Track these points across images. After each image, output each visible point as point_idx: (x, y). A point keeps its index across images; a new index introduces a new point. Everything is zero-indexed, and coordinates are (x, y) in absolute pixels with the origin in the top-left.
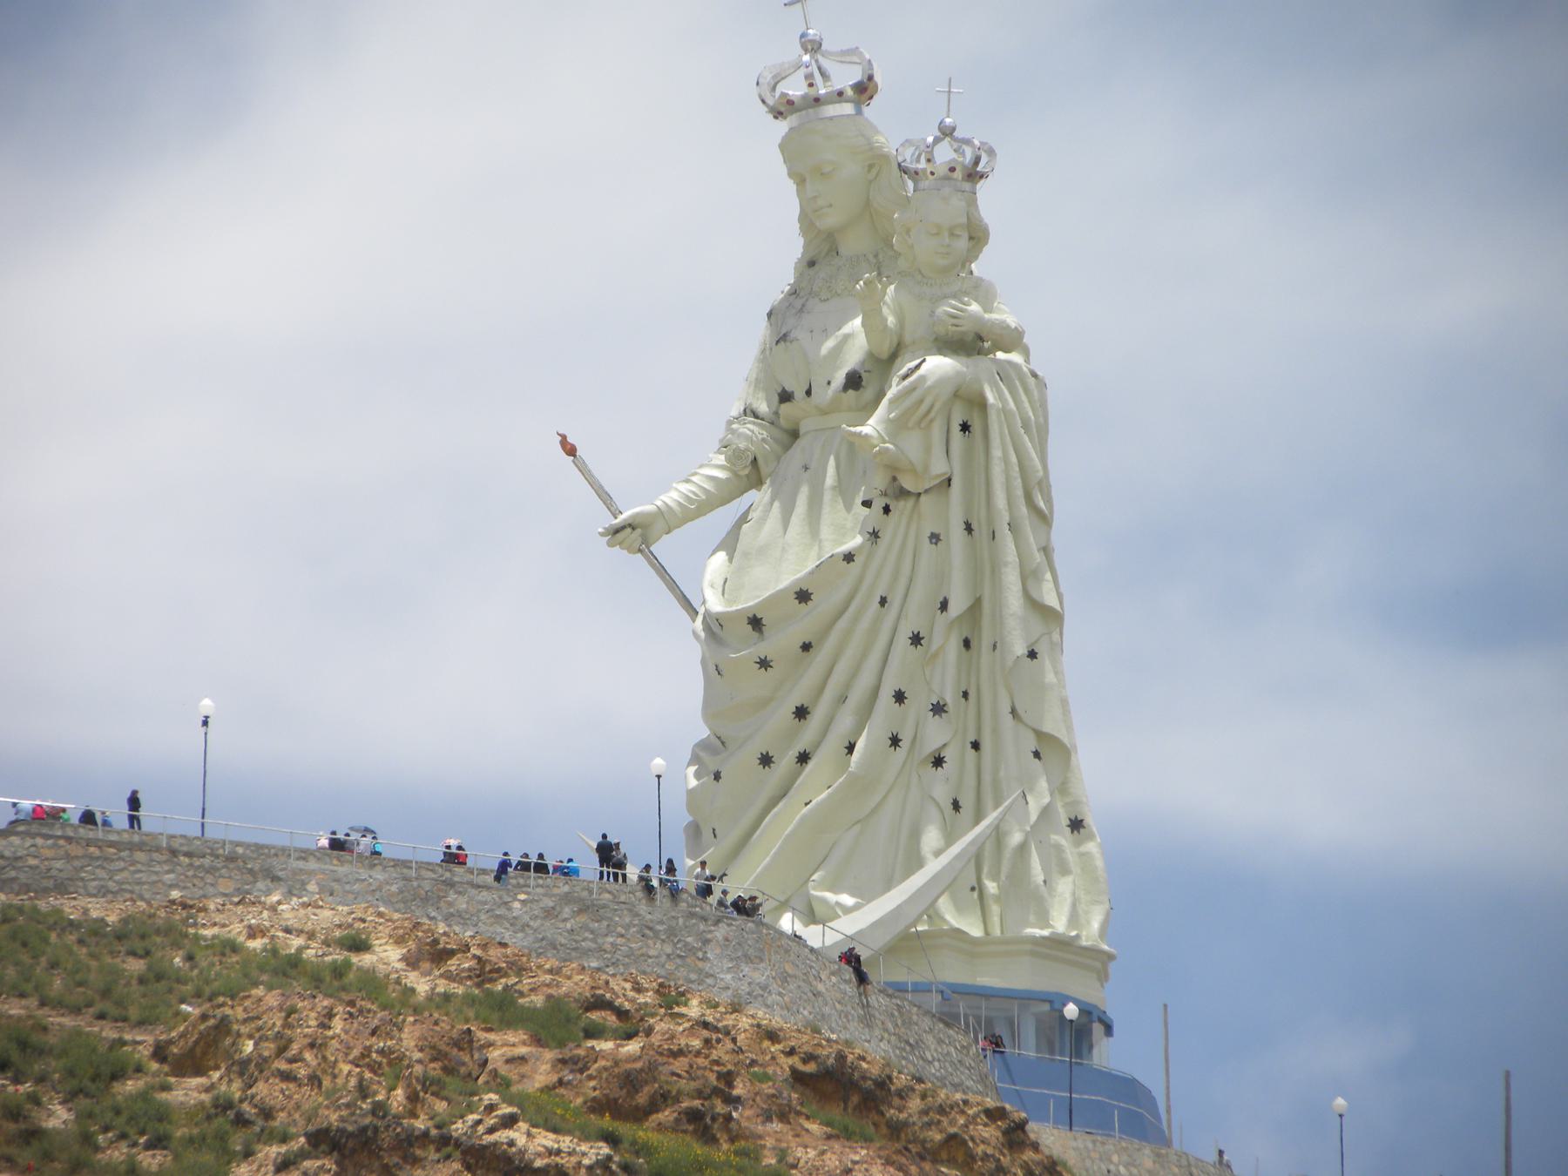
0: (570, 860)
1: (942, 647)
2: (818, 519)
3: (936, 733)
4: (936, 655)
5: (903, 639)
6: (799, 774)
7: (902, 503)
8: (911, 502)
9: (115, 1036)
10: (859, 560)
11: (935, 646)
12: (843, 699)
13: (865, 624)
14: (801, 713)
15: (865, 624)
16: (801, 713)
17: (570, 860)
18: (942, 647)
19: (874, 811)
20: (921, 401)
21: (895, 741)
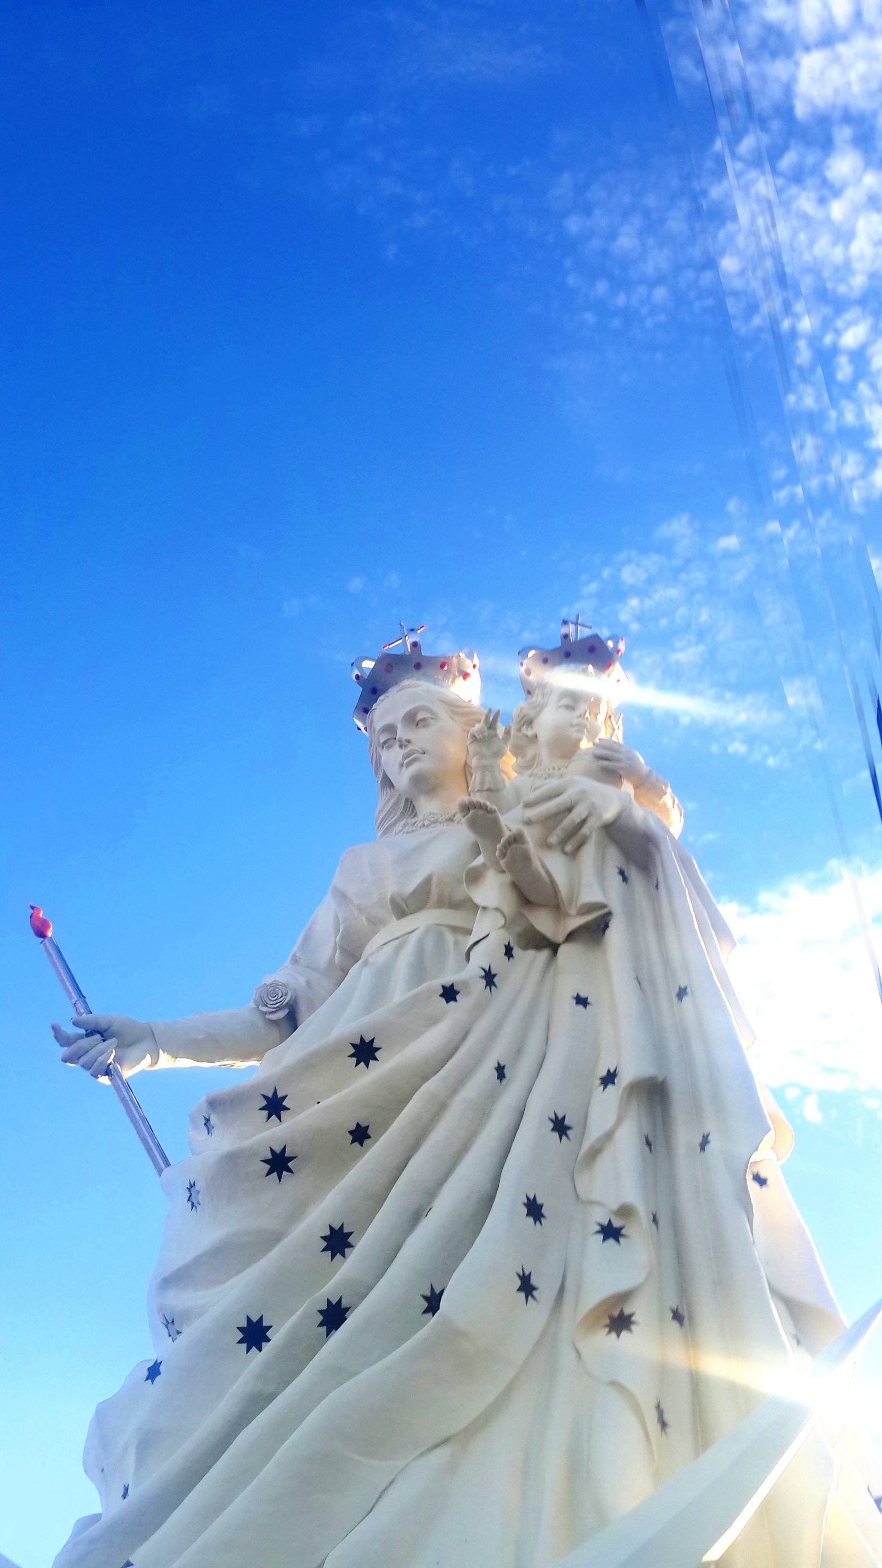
0: (761, 1181)
1: (609, 1136)
2: (868, 759)
3: (606, 1272)
4: (595, 1153)
5: (534, 1127)
6: (313, 1350)
7: (531, 953)
8: (545, 954)
9: (803, 289)
10: (463, 1002)
11: (595, 1132)
12: (416, 1217)
13: (471, 1090)
14: (337, 1242)
15: (471, 1090)
16: (337, 1242)
17: (761, 1181)
18: (609, 1136)
19: (472, 1431)
20: (570, 810)
21: (527, 1287)
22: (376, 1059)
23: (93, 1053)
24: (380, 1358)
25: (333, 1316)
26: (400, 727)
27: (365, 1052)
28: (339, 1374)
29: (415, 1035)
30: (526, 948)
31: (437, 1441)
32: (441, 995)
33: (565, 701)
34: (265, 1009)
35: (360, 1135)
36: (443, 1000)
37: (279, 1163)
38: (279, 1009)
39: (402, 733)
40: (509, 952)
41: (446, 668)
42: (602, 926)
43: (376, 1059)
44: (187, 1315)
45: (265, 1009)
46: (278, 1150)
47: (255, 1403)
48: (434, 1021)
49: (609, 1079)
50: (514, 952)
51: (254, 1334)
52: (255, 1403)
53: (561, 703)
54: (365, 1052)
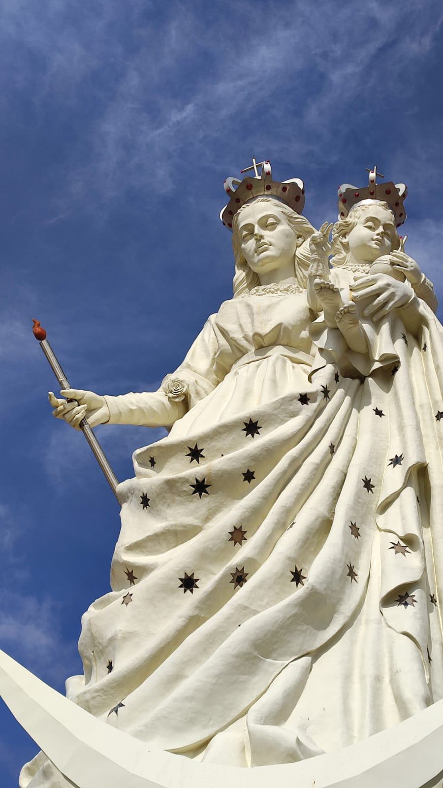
1: (397, 495)
8: (357, 382)
16: (238, 535)
18: (397, 495)
22: (258, 433)
23: (74, 411)
24: (269, 605)
25: (239, 577)
26: (256, 227)
27: (252, 427)
28: (245, 611)
29: (283, 421)
30: (345, 377)
31: (305, 653)
32: (299, 400)
33: (370, 224)
34: (171, 395)
35: (249, 476)
36: (300, 403)
37: (201, 487)
38: (178, 396)
39: (257, 230)
40: (336, 378)
41: (357, 193)
42: (392, 369)
43: (258, 433)
44: (145, 570)
45: (171, 395)
46: (200, 479)
47: (193, 622)
48: (294, 415)
49: (397, 461)
50: (339, 379)
51: (189, 583)
52: (193, 622)
53: (367, 225)
54: (252, 427)
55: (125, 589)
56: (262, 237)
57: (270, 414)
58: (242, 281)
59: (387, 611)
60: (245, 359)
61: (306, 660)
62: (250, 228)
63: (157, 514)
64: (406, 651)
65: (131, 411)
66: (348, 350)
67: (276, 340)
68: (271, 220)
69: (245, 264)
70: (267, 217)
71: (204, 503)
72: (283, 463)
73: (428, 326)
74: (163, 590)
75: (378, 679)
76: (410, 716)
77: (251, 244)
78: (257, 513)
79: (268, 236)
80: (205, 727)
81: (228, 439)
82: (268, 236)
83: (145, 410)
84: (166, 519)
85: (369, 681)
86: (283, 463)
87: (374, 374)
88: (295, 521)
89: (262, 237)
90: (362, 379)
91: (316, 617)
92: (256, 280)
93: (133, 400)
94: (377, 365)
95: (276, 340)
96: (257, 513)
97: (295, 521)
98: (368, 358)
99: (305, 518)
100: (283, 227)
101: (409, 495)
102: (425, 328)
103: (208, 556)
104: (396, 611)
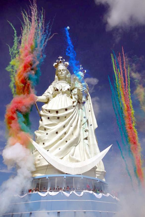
1: (85, 123)
18: (85, 123)
27: (66, 110)
44: (48, 129)
54: (66, 110)
55: (96, 131)
56: (62, 73)
57: (69, 108)
58: (57, 78)
59: (84, 140)
60: (60, 94)
61: (75, 147)
62: (60, 71)
63: (51, 121)
64: (87, 146)
65: (41, 100)
66: (79, 98)
67: (66, 92)
68: (64, 70)
69: (57, 75)
70: (64, 69)
71: (58, 120)
72: (71, 116)
73: (89, 96)
74: (53, 133)
75: (84, 150)
76: (38, 144)
77: (60, 73)
78: (67, 123)
79: (63, 72)
80: (63, 155)
81: (62, 111)
82: (63, 72)
83: (19, 86)
84: (52, 122)
85: (83, 150)
86: (71, 116)
87: (82, 103)
88: (72, 125)
89: (62, 73)
90: (80, 103)
91: (76, 142)
92: (59, 79)
93: (42, 98)
94: (83, 102)
95: (66, 92)
96: (67, 123)
97: (72, 125)
98: (81, 100)
99: (74, 125)
100: (65, 71)
101: (86, 123)
102: (88, 96)
103: (61, 129)
104: (86, 141)
